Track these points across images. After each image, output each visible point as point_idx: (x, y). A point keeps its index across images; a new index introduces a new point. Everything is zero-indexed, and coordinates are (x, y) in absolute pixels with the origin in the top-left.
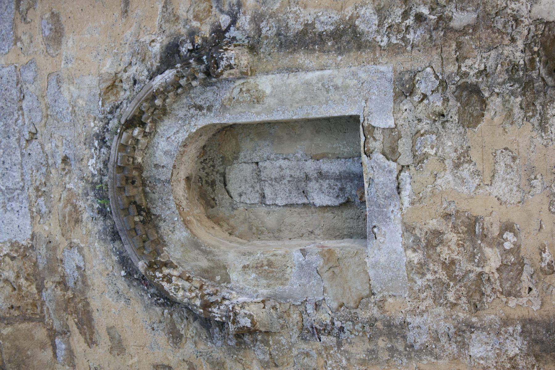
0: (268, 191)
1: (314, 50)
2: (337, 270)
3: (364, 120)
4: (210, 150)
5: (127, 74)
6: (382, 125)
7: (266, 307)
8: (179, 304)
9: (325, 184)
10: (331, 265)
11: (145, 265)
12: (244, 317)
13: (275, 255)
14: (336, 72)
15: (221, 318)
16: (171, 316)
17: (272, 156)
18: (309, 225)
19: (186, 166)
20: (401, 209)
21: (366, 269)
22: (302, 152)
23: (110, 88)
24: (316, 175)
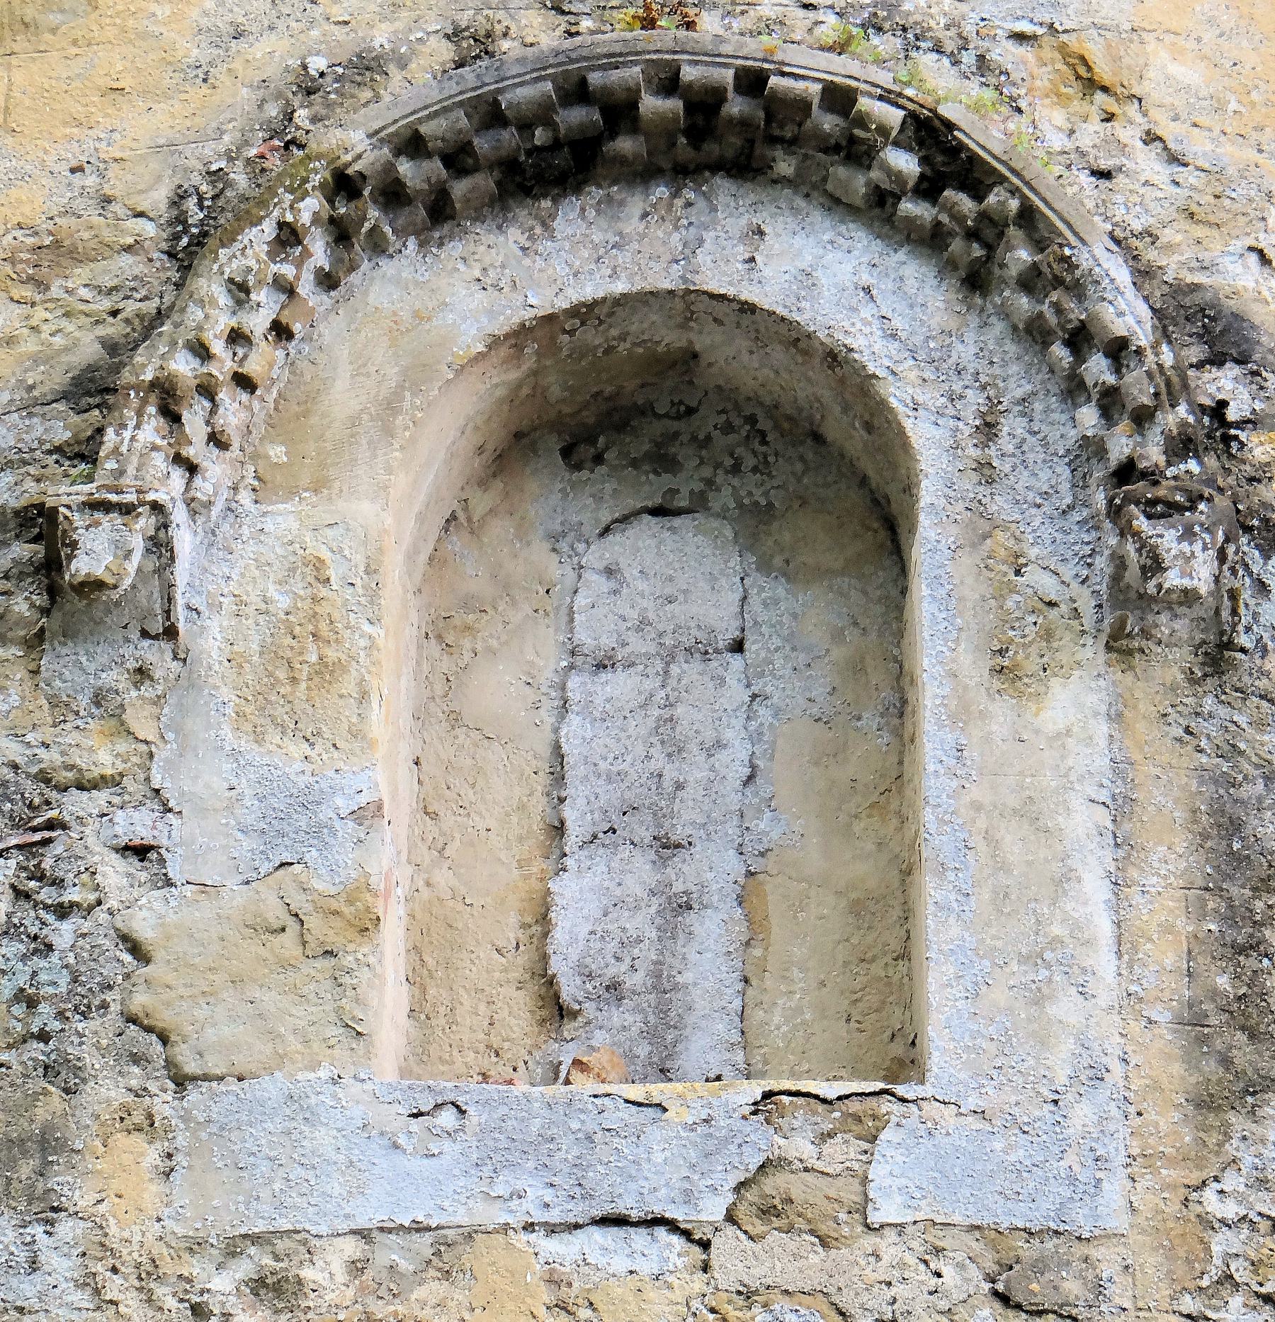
0: (619, 687)
1: (1202, 917)
2: (288, 941)
3: (903, 1100)
4: (802, 458)
5: (1140, 144)
6: (876, 1172)
7: (146, 643)
8: (179, 286)
9: (641, 923)
10: (312, 922)
11: (349, 158)
12: (116, 544)
13: (364, 696)
14: (1105, 998)
15: (116, 451)
16: (128, 249)
17: (764, 713)
18: (472, 844)
19: (745, 357)
20: (529, 1227)
21: (289, 1067)
22: (775, 835)
23: (1082, 71)
24: (678, 887)
